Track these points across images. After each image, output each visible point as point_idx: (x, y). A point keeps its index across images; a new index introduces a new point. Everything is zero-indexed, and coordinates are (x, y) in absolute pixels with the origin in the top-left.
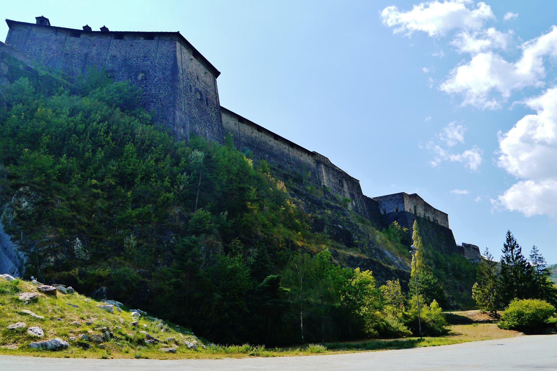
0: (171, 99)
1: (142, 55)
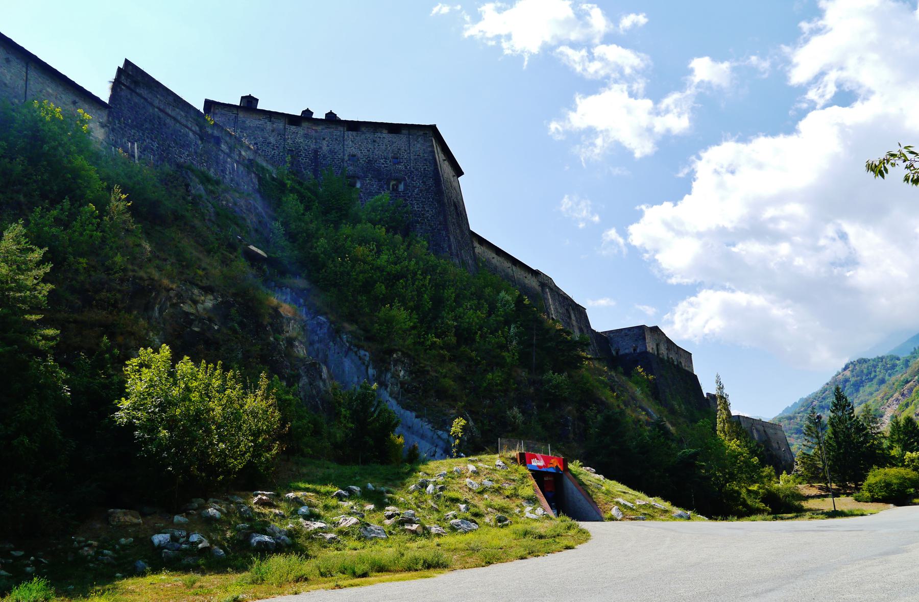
0: (441, 218)
1: (390, 155)
